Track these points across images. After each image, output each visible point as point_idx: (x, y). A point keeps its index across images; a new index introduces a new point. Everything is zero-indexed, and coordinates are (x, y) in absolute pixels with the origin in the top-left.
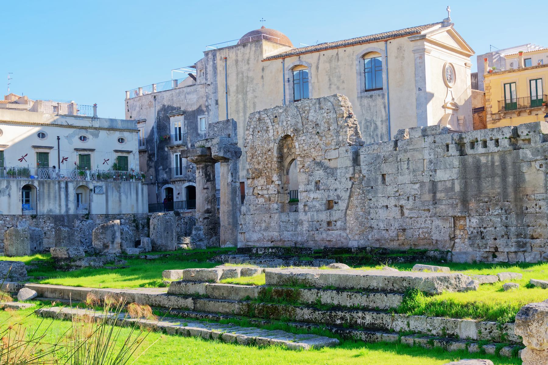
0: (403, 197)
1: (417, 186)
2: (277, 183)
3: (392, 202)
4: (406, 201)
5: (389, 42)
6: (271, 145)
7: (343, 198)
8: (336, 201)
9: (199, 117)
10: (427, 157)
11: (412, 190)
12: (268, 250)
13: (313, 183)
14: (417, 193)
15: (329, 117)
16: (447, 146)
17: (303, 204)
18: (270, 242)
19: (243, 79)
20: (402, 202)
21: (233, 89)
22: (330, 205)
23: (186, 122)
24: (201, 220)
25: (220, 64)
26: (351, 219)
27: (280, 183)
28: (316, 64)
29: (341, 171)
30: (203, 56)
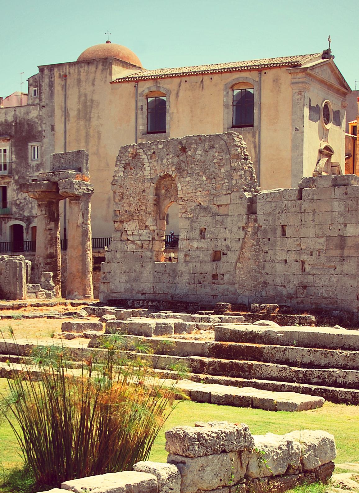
0: (306, 251)
1: (322, 240)
2: (152, 228)
3: (291, 257)
4: (309, 256)
5: (264, 72)
6: (147, 184)
7: (233, 249)
8: (225, 252)
9: (30, 144)
10: (336, 209)
11: (317, 244)
12: (148, 302)
13: (198, 232)
14: (322, 247)
15: (220, 158)
17: (184, 253)
18: (140, 295)
19: (86, 102)
20: (304, 257)
21: (73, 113)
22: (217, 256)
23: (13, 149)
24: (42, 265)
25: (58, 82)
26: (242, 273)
27: (155, 228)
28: (175, 92)
29: (232, 219)
30: (37, 71)
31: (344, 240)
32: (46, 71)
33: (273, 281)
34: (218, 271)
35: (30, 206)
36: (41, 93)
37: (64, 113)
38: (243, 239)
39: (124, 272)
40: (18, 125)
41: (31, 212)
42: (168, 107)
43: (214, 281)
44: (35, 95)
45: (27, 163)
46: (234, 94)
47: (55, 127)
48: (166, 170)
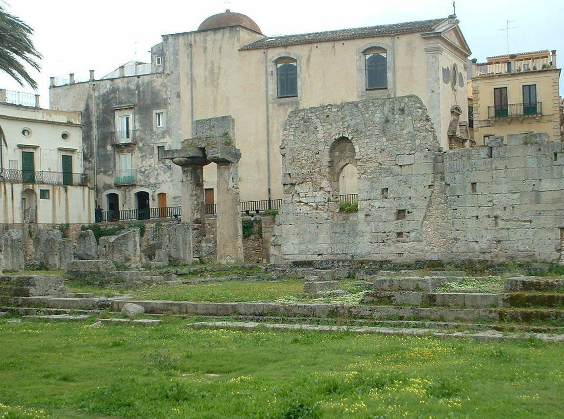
1: (516, 196)
13: (379, 192)
16: (556, 155)
19: (213, 70)
21: (199, 81)
22: (401, 214)
30: (160, 40)
31: (539, 195)
32: (170, 40)
33: (464, 237)
34: (403, 230)
35: (156, 173)
36: (165, 62)
37: (190, 81)
38: (430, 197)
39: (298, 234)
40: (141, 93)
41: (157, 179)
42: (299, 72)
43: (398, 239)
44: (159, 63)
45: (152, 130)
46: (366, 59)
47: (181, 94)
48: (341, 133)
